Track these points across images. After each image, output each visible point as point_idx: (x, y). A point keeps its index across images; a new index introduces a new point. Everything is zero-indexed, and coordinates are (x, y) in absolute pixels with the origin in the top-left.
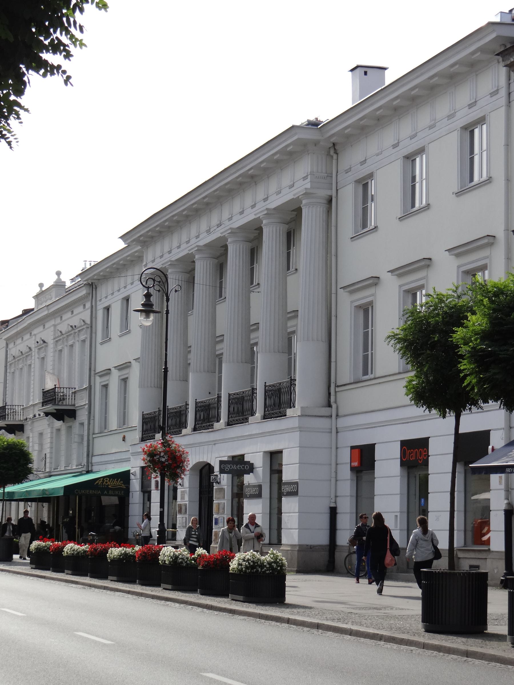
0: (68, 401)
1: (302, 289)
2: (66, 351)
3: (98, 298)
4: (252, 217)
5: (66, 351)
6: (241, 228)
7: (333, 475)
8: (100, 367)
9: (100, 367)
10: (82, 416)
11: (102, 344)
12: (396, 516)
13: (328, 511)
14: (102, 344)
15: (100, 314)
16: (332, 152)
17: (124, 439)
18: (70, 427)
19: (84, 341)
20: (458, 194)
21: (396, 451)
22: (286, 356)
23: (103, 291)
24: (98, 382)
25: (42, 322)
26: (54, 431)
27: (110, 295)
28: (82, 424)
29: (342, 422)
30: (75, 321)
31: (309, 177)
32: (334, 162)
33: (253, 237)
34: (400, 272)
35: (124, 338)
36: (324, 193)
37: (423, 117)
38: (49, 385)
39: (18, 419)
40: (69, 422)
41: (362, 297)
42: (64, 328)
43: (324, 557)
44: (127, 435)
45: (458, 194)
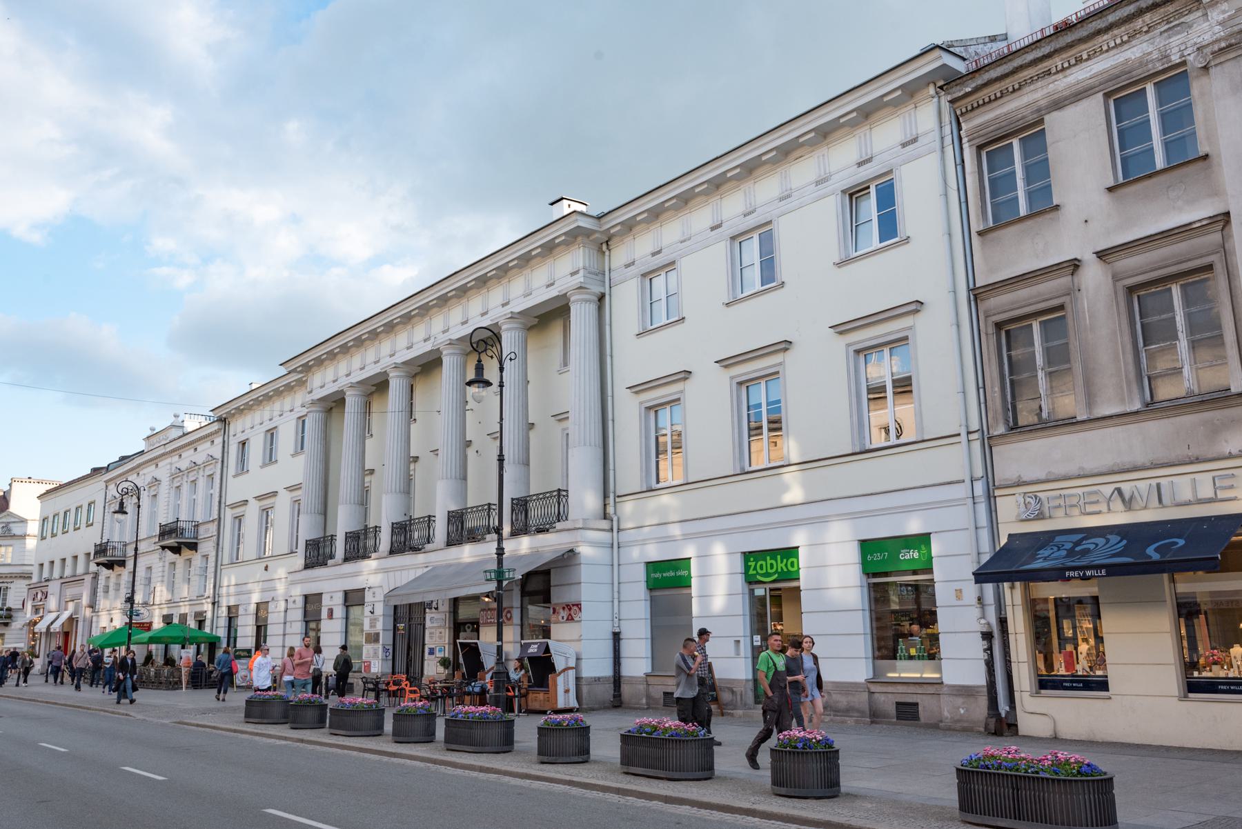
0: (118, 553)
1: (573, 388)
2: (186, 488)
3: (232, 433)
4: (428, 347)
5: (186, 488)
6: (320, 400)
7: (616, 595)
8: (231, 498)
9: (231, 498)
10: (207, 547)
11: (234, 476)
12: (738, 642)
13: (611, 636)
14: (234, 476)
15: (233, 449)
16: (604, 247)
17: (266, 568)
18: (190, 560)
19: (211, 476)
20: (293, 456)
21: (640, 574)
22: (320, 518)
23: (238, 427)
24: (229, 515)
25: (155, 461)
26: (167, 564)
27: (249, 427)
28: (206, 557)
29: (624, 537)
30: (200, 458)
31: (581, 273)
32: (607, 258)
33: (378, 386)
34: (259, 498)
35: (240, 478)
36: (598, 290)
37: (277, 406)
38: (165, 518)
39: (188, 537)
40: (186, 553)
41: (238, 511)
42: (184, 464)
43: (607, 692)
44: (270, 564)
45: (293, 456)
